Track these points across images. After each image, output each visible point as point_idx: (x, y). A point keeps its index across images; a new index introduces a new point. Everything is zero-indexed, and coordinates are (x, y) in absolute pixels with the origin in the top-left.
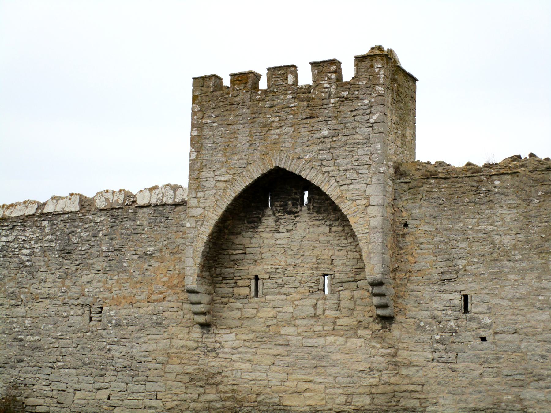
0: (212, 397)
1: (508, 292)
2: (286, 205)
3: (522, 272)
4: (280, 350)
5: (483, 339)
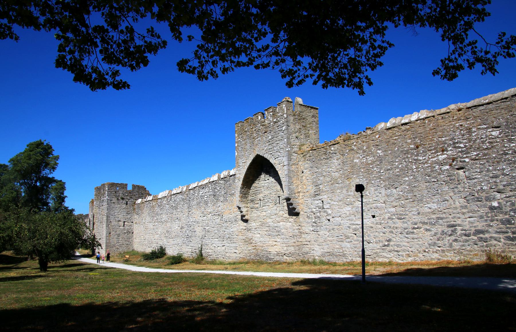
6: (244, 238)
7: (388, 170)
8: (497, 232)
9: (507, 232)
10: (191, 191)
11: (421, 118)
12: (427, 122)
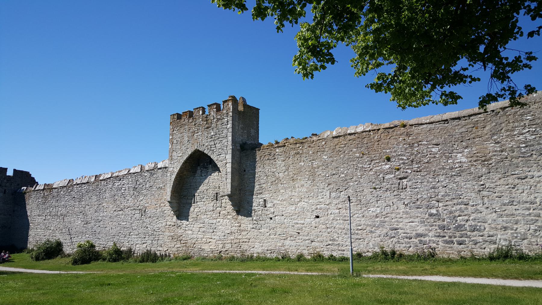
0: (179, 246)
1: (280, 198)
2: (204, 165)
3: (285, 189)
4: (202, 225)
5: (271, 219)
6: (172, 234)
7: (334, 174)
8: (435, 236)
9: (444, 237)
10: (103, 182)
11: (366, 130)
12: (372, 134)
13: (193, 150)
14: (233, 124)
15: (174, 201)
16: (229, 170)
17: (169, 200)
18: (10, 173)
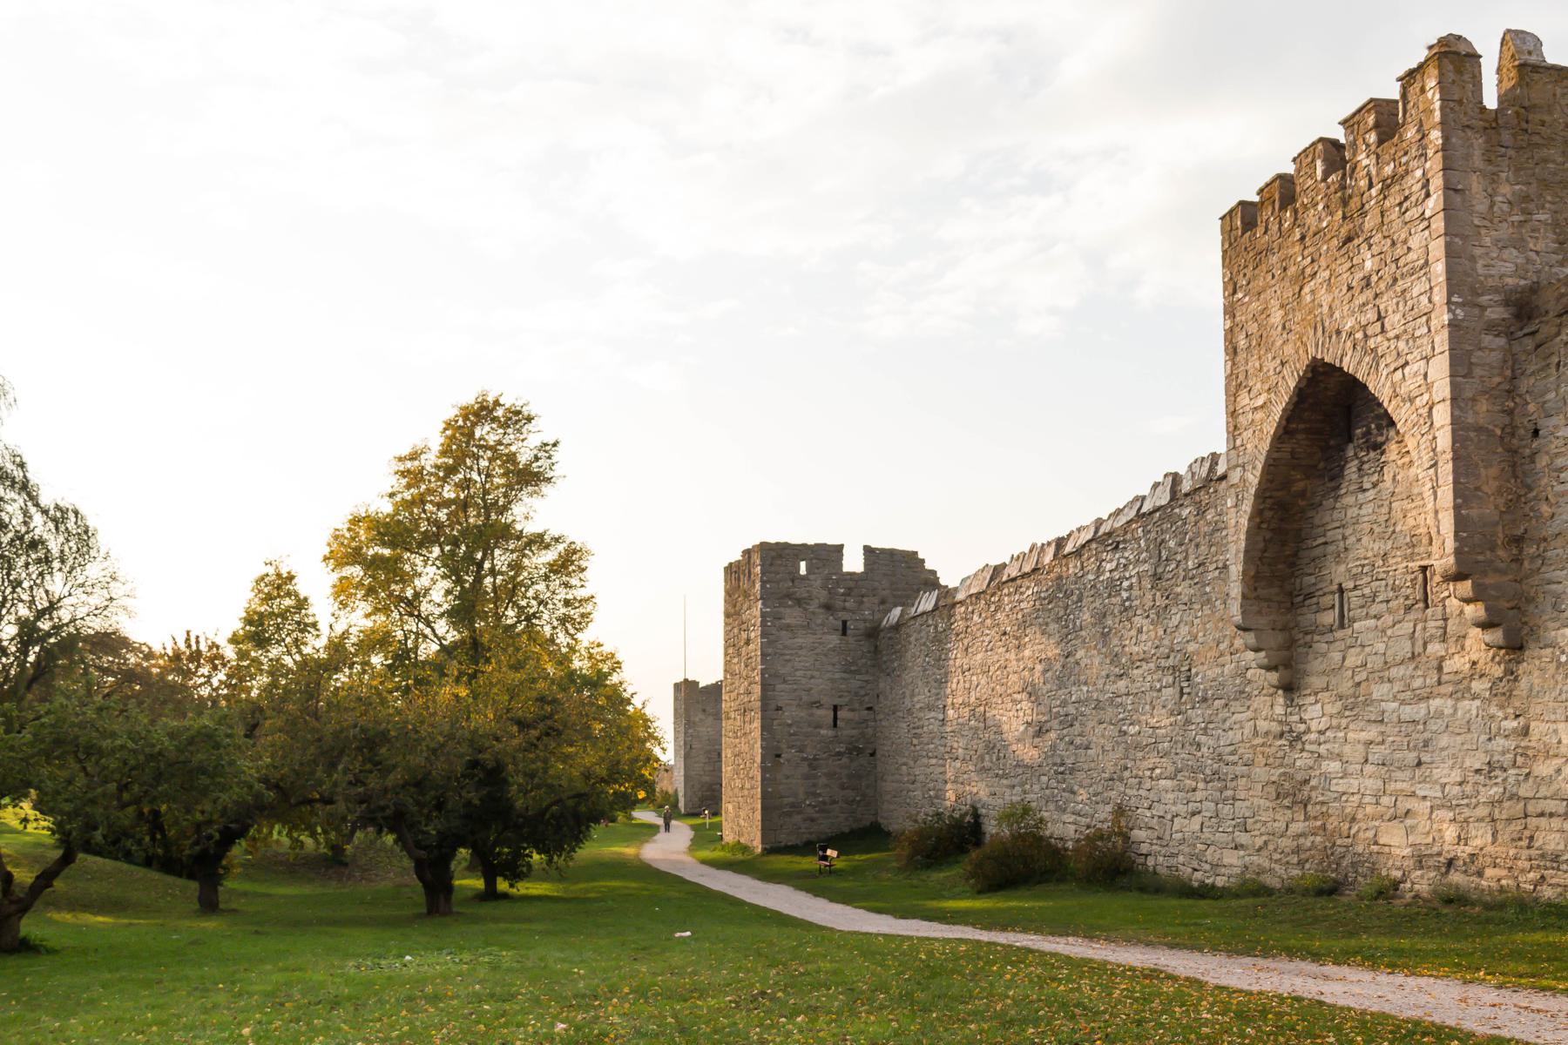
4: (1372, 733)
13: (1302, 366)
14: (1449, 188)
15: (1262, 621)
16: (1444, 440)
17: (1238, 619)
18: (853, 563)
